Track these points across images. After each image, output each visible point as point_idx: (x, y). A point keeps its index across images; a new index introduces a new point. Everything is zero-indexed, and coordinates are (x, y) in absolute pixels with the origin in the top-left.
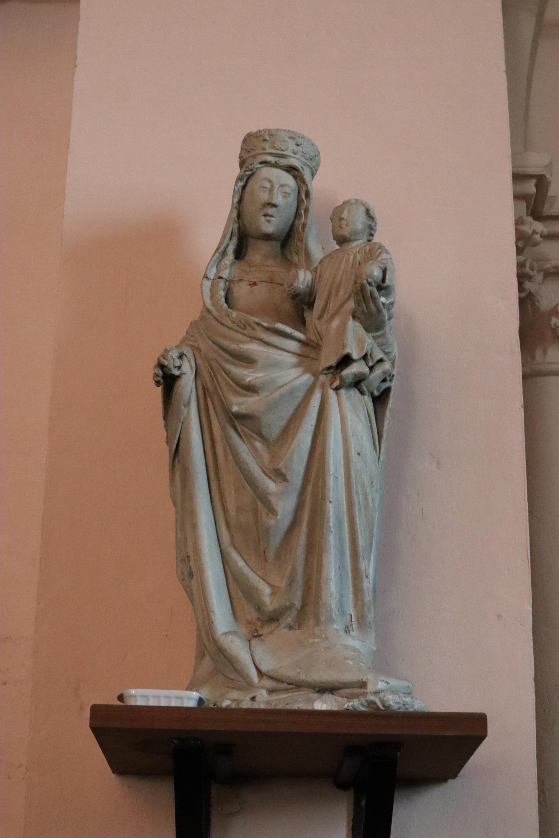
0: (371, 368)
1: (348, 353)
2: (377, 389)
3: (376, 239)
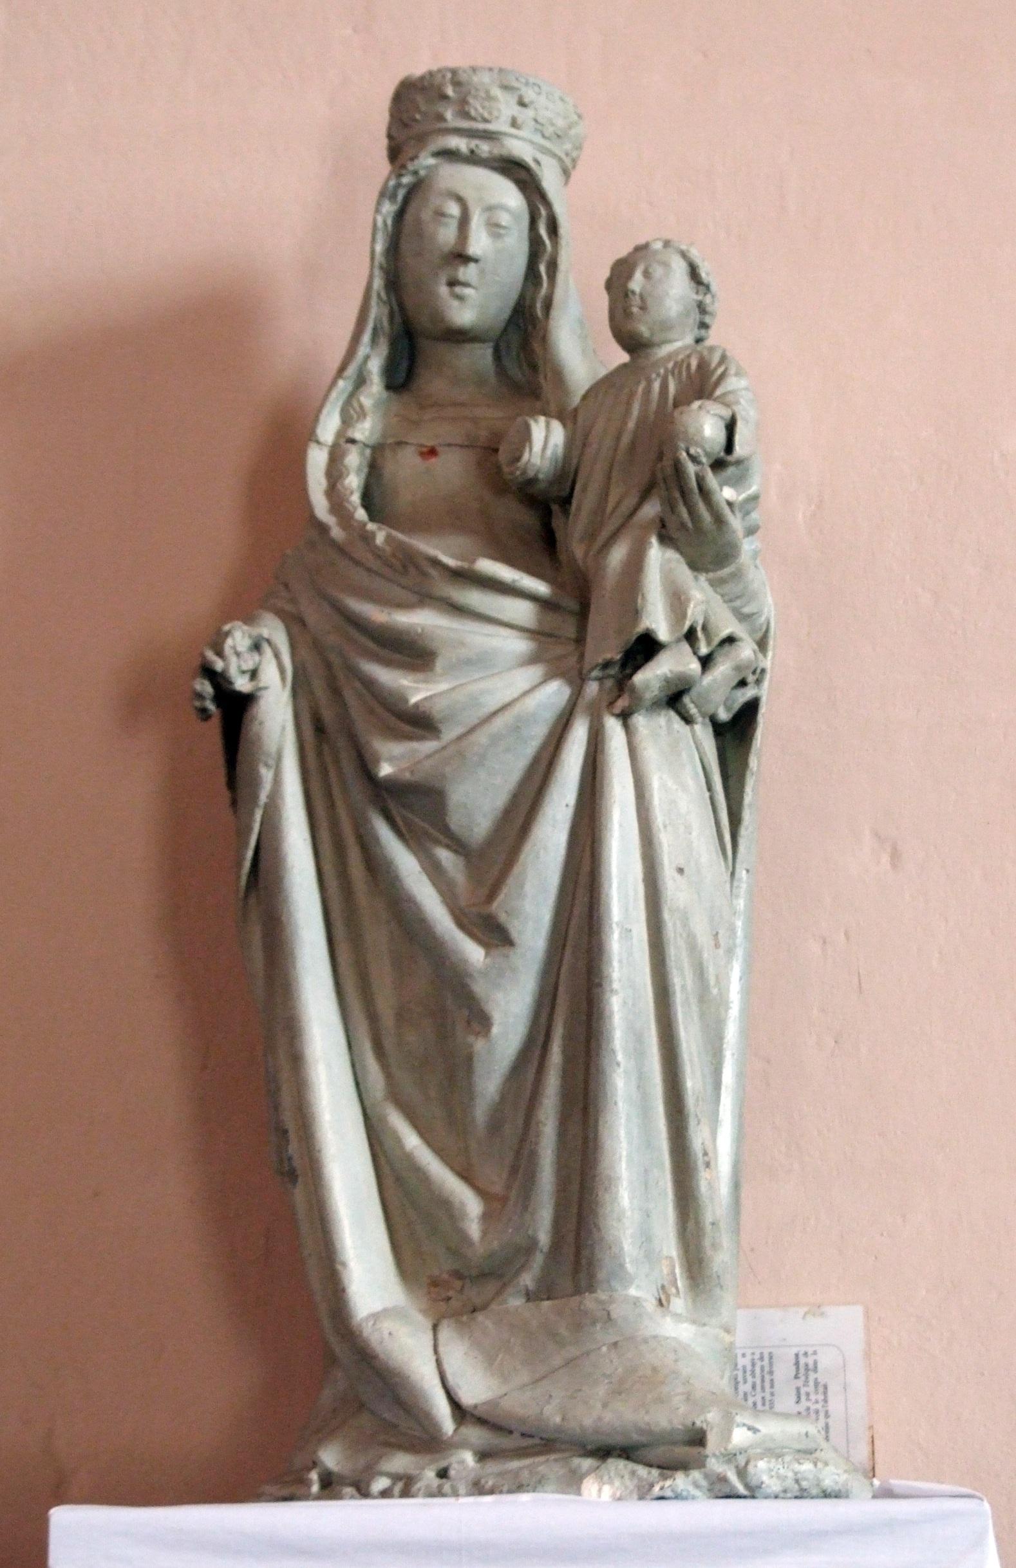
0: (706, 662)
1: (648, 629)
2: (725, 704)
3: (714, 338)
